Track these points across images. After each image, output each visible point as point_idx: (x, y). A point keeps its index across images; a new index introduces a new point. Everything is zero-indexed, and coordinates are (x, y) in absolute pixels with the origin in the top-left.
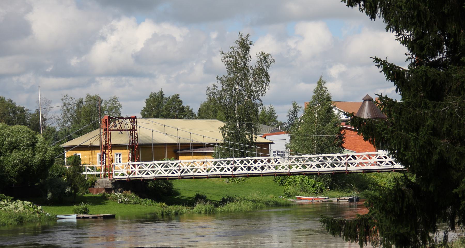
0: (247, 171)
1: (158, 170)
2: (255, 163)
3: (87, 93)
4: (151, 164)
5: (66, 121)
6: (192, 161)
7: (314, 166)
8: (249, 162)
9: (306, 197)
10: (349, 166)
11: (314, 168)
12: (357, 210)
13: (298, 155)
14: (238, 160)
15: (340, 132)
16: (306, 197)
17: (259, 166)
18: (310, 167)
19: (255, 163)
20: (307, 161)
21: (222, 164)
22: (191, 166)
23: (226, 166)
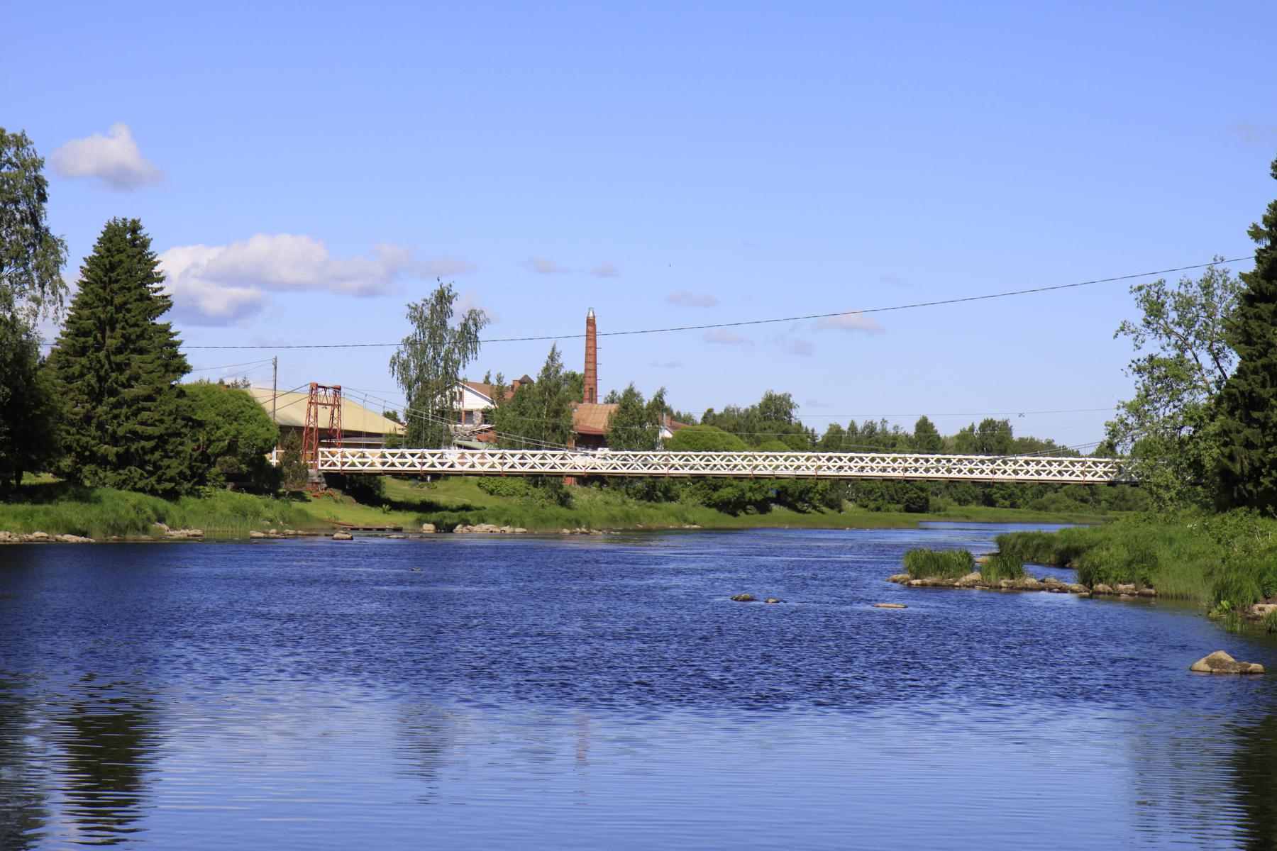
0: (902, 473)
1: (632, 465)
2: (850, 462)
3: (667, 388)
4: (642, 456)
5: (28, 336)
6: (751, 453)
7: (1010, 472)
8: (906, 461)
9: (317, 820)
10: (1041, 474)
11: (1032, 475)
12: (1253, 774)
13: (919, 453)
14: (803, 457)
15: (112, 298)
16: (317, 820)
17: (436, 454)
18: (1048, 474)
19: (850, 462)
20: (976, 465)
21: (778, 460)
22: (707, 461)
23: (805, 463)
